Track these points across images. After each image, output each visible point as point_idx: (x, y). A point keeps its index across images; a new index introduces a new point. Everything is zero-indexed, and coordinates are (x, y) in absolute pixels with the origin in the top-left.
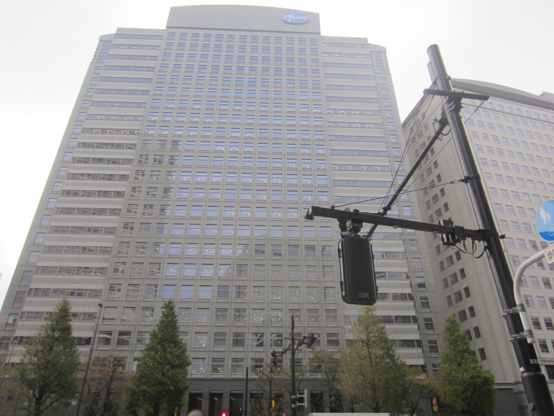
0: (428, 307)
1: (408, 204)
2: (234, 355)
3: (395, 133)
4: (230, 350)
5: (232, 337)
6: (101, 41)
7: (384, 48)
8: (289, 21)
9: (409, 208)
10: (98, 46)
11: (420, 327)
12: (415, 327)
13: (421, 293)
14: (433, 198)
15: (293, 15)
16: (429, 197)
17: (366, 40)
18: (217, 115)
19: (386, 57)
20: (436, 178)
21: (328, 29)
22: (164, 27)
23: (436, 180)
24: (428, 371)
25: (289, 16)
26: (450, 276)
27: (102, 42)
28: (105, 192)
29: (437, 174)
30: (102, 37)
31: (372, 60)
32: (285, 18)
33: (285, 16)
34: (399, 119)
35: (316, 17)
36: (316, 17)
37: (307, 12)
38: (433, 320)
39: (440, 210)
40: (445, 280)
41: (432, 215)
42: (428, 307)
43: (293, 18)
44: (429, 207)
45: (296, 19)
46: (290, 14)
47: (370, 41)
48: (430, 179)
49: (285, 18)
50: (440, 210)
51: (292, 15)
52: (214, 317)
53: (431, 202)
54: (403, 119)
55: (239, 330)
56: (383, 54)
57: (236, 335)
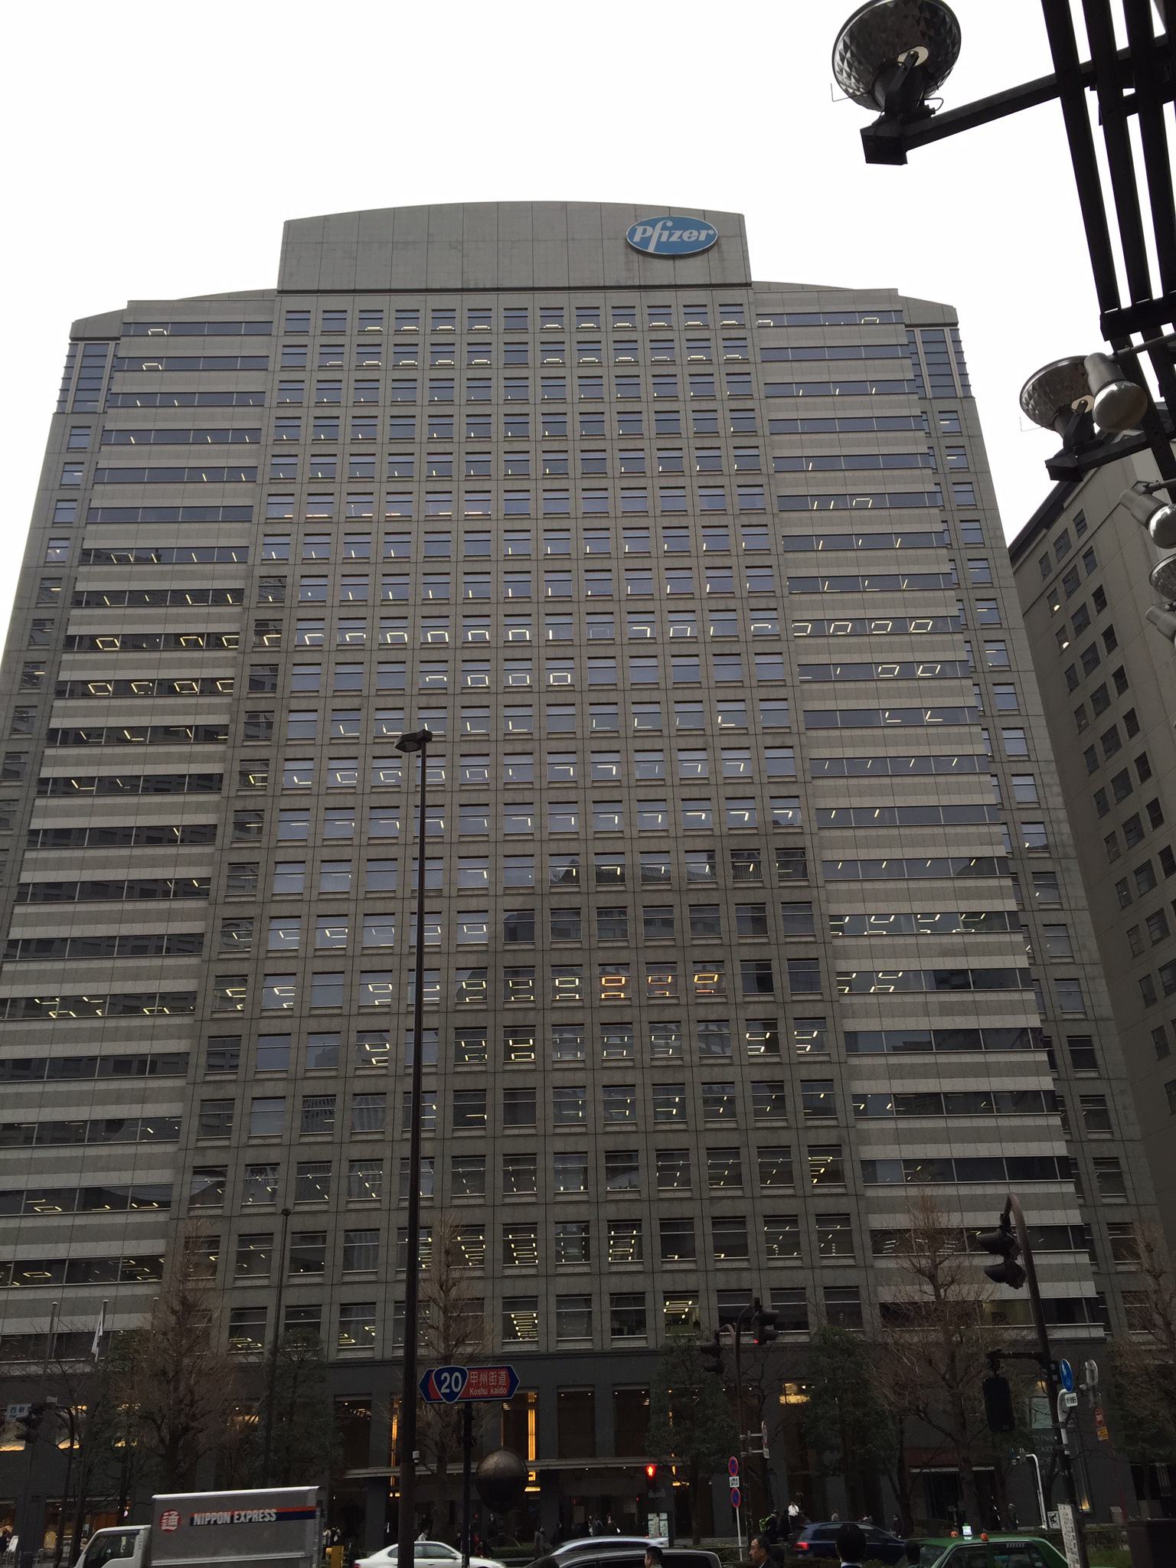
0: (1121, 1189)
1: (1038, 816)
2: (511, 1147)
3: (983, 554)
4: (498, 1201)
5: (500, 1099)
6: (75, 339)
7: (951, 311)
8: (651, 249)
9: (1029, 780)
10: (71, 357)
11: (1059, 1061)
12: (1056, 1121)
13: (1086, 1081)
14: (1104, 738)
15: (664, 228)
16: (1104, 778)
17: (891, 294)
18: (428, 345)
19: (957, 342)
20: (1092, 599)
21: (768, 263)
22: (269, 281)
23: (1092, 607)
24: (1112, 1313)
25: (649, 229)
26: (1161, 970)
27: (82, 344)
28: (74, 1264)
29: (1094, 588)
30: (78, 325)
31: (917, 365)
32: (637, 238)
33: (640, 229)
34: (998, 527)
35: (734, 224)
36: (734, 224)
37: (704, 213)
38: (1123, 1162)
39: (1124, 775)
40: (1101, 793)
41: (1092, 748)
42: (1121, 1189)
43: (664, 239)
44: (1093, 765)
45: (674, 238)
46: (652, 223)
47: (900, 294)
48: (1104, 723)
49: (637, 238)
50: (1124, 775)
51: (660, 225)
52: (448, 1177)
53: (1100, 749)
54: (1011, 531)
55: (519, 1082)
56: (947, 330)
57: (510, 1093)
